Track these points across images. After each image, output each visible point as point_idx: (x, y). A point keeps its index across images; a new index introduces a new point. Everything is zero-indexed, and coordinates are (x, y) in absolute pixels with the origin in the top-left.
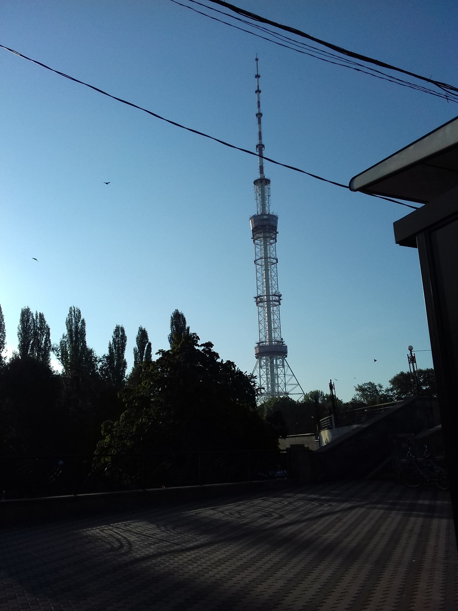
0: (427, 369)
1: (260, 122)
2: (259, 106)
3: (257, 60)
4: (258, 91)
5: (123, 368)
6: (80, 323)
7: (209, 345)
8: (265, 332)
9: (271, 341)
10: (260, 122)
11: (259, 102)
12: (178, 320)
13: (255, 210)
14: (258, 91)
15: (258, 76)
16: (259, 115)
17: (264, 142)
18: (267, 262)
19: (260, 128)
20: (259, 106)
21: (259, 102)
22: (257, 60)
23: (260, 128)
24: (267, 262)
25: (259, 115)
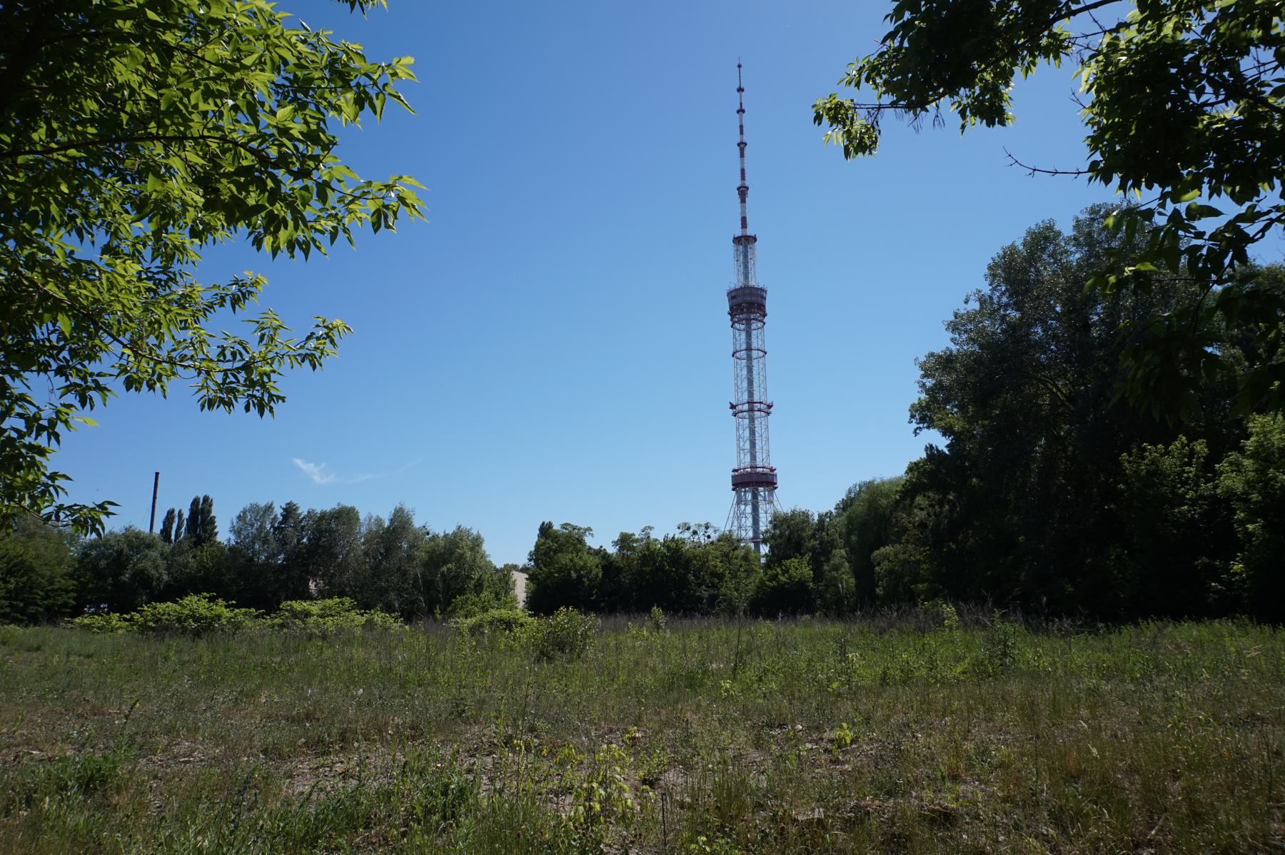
0: (793, 512)
1: (742, 155)
2: (742, 132)
3: (739, 66)
4: (741, 111)
5: (1224, 231)
6: (1190, 55)
7: (625, 541)
8: (747, 460)
9: (755, 496)
10: (742, 155)
11: (741, 127)
12: (262, 415)
13: (734, 280)
14: (741, 111)
15: (740, 90)
16: (742, 145)
17: (747, 183)
18: (748, 354)
19: (742, 163)
20: (742, 132)
21: (741, 127)
22: (739, 66)
23: (742, 163)
24: (748, 354)
25: (742, 145)
